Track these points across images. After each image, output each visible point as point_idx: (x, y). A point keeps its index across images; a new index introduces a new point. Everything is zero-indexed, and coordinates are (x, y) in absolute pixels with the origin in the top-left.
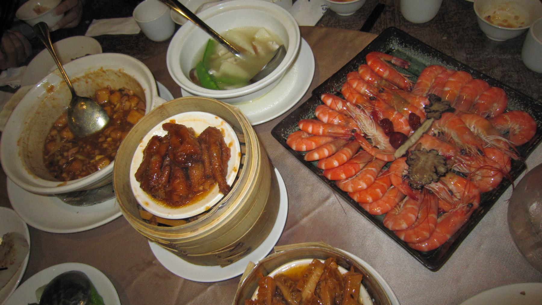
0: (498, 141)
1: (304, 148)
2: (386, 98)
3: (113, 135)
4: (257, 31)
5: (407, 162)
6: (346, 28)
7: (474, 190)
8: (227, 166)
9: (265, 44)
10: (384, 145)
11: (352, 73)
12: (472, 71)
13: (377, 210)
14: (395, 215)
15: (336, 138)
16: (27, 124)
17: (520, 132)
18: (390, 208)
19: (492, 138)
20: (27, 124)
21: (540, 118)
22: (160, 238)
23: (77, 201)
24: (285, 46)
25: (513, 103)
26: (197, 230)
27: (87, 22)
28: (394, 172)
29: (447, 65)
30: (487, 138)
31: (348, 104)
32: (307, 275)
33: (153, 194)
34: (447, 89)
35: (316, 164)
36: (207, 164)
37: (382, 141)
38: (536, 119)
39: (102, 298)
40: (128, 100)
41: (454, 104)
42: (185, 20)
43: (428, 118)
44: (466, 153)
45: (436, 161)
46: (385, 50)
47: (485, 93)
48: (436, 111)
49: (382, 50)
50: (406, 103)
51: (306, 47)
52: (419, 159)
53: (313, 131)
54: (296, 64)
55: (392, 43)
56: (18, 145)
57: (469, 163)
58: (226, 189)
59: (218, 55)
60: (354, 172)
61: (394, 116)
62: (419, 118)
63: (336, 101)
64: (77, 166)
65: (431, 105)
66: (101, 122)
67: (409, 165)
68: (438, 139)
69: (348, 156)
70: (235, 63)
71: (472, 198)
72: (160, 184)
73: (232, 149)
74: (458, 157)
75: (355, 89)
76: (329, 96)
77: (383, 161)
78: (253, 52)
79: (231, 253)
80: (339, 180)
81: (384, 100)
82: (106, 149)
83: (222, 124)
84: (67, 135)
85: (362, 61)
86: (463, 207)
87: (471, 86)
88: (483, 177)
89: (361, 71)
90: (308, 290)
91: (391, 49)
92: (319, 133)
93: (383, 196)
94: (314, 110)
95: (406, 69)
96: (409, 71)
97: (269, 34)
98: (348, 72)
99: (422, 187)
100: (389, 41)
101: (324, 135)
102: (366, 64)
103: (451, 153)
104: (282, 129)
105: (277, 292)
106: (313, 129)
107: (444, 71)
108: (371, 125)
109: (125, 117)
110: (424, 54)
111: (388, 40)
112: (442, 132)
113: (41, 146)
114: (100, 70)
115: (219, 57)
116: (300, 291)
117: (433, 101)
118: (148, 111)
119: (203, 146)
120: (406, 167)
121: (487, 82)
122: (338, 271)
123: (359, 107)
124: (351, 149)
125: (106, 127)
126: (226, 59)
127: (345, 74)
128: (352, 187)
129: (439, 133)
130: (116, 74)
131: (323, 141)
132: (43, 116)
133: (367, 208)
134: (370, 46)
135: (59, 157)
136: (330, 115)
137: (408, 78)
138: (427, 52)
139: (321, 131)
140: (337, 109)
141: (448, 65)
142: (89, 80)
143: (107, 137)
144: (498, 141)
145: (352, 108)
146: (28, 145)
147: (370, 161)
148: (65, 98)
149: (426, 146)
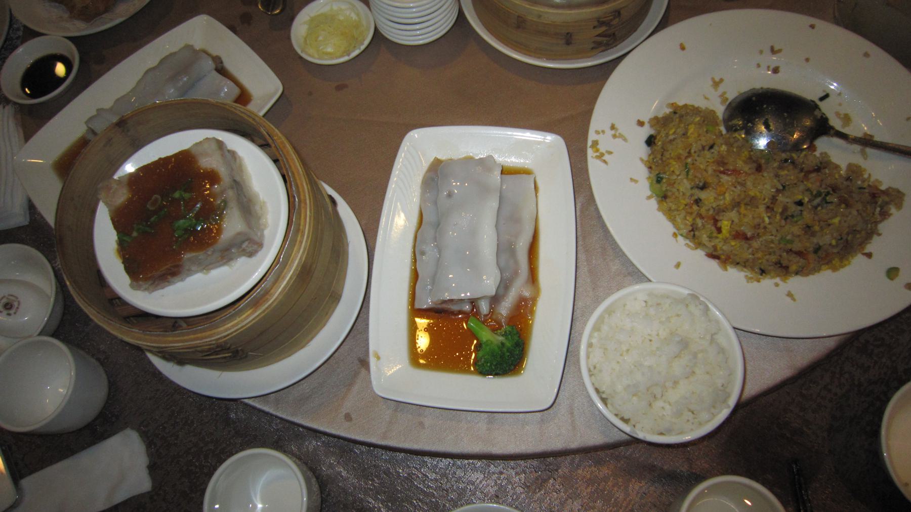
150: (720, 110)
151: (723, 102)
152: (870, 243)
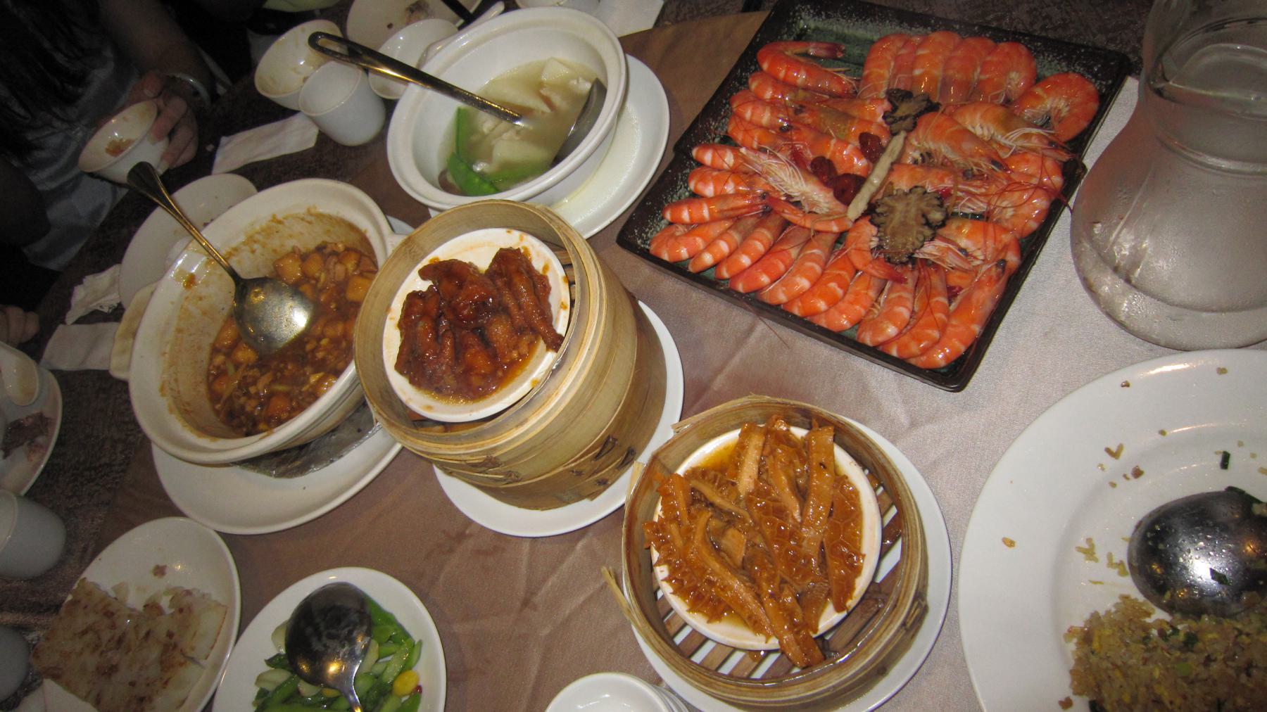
0: (1027, 136)
1: (684, 253)
2: (810, 121)
3: (330, 332)
4: (542, 68)
5: (872, 222)
6: (714, 14)
7: (1003, 236)
8: (549, 306)
9: (563, 88)
10: (826, 205)
11: (739, 93)
12: (958, 27)
13: (843, 322)
14: (873, 319)
15: (736, 218)
16: (167, 356)
17: (1069, 111)
18: (863, 312)
19: (1016, 134)
20: (167, 356)
21: (1100, 75)
22: (467, 454)
23: (298, 467)
24: (602, 80)
25: (1046, 62)
26: (526, 421)
27: (210, 148)
28: (853, 246)
29: (910, 30)
30: (1007, 138)
31: (743, 150)
32: (738, 452)
33: (435, 385)
34: (917, 72)
35: (711, 274)
36: (515, 311)
37: (821, 200)
38: (1093, 80)
39: (392, 615)
40: (340, 262)
41: (938, 96)
42: (402, 86)
43: (893, 134)
44: (974, 176)
45: (923, 205)
46: (791, 35)
47: (989, 58)
48: (903, 118)
49: (785, 36)
50: (847, 117)
51: (637, 65)
52: (892, 210)
53: (691, 218)
54: (630, 106)
55: (801, 18)
56: (163, 395)
57: (983, 190)
58: (555, 342)
59: (483, 132)
60: (782, 267)
61: (831, 150)
62: (877, 139)
63: (720, 152)
64: (278, 404)
65: (895, 109)
66: (298, 319)
67: (878, 226)
68: (922, 166)
69: (765, 241)
70: (517, 138)
71: (1002, 250)
72: (442, 365)
73: (549, 275)
74: (960, 186)
75: (750, 122)
76: (706, 147)
77: (832, 232)
78: (546, 109)
79: (600, 461)
80: (761, 289)
81: (808, 126)
82: (324, 360)
83: (521, 239)
84: (245, 355)
85: (753, 68)
86: (990, 269)
87: (959, 53)
88: (1016, 207)
89: (754, 86)
90: (746, 480)
91: (802, 30)
92: (703, 218)
93: (845, 294)
94: (686, 182)
95: (839, 59)
96: (845, 61)
97: (568, 67)
98: (732, 95)
99: (912, 259)
100: (794, 16)
101: (714, 220)
102: (761, 70)
103: (948, 183)
104: (636, 231)
105: (696, 499)
106: (690, 214)
107: (907, 42)
108: (794, 176)
109: (342, 295)
110: (865, 20)
111: (791, 14)
112: (927, 153)
113: (203, 389)
114: (272, 221)
115: (484, 136)
116: (733, 484)
117: (897, 101)
118: (381, 261)
119: (499, 283)
120: (874, 230)
121: (989, 38)
122: (793, 435)
123: (764, 151)
124: (769, 229)
125: (312, 322)
126: (500, 135)
127: (726, 99)
128: (783, 292)
129: (921, 155)
130: (303, 219)
131: (716, 229)
132: (190, 335)
133: (823, 323)
134: (759, 35)
135: (243, 400)
136: (716, 181)
137: (844, 72)
138: (867, 17)
139: (706, 213)
140: (726, 166)
141: (913, 29)
142: (256, 246)
143: (319, 339)
144: (1027, 136)
145: (752, 156)
146: (179, 392)
147: (808, 241)
148: (220, 292)
149: (902, 183)
150: (1128, 586)
151: (1122, 573)
152: (366, 231)
